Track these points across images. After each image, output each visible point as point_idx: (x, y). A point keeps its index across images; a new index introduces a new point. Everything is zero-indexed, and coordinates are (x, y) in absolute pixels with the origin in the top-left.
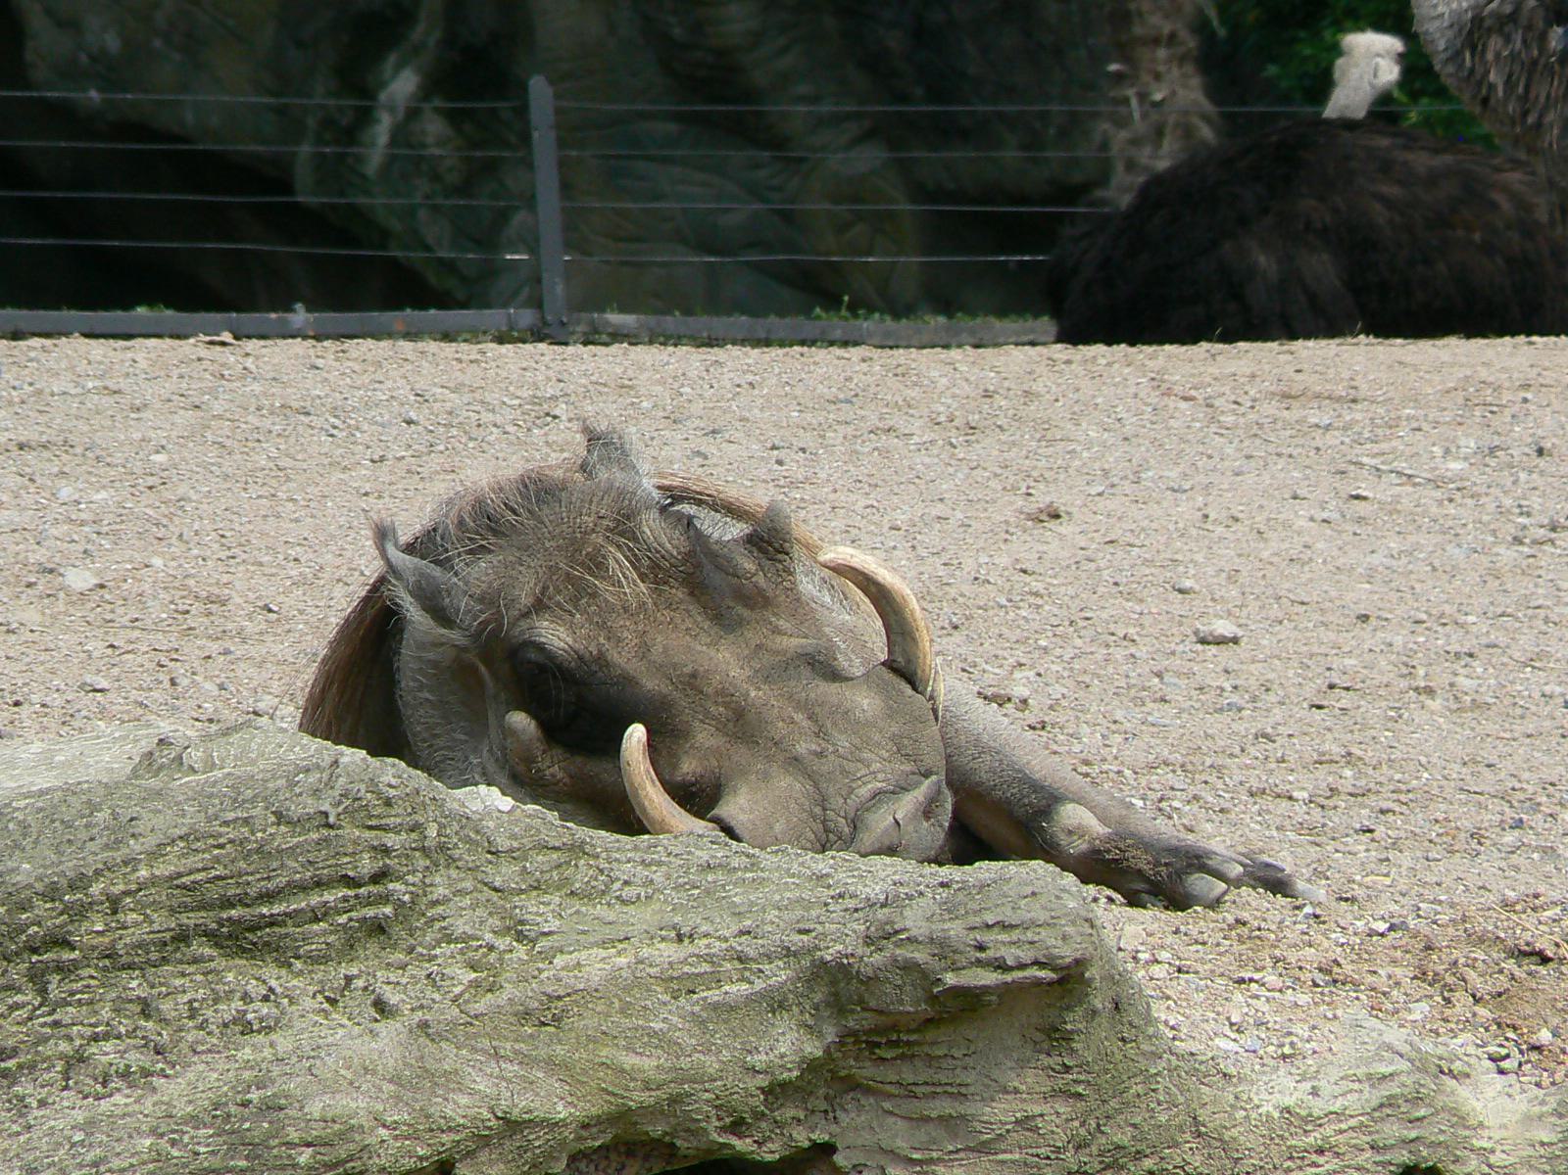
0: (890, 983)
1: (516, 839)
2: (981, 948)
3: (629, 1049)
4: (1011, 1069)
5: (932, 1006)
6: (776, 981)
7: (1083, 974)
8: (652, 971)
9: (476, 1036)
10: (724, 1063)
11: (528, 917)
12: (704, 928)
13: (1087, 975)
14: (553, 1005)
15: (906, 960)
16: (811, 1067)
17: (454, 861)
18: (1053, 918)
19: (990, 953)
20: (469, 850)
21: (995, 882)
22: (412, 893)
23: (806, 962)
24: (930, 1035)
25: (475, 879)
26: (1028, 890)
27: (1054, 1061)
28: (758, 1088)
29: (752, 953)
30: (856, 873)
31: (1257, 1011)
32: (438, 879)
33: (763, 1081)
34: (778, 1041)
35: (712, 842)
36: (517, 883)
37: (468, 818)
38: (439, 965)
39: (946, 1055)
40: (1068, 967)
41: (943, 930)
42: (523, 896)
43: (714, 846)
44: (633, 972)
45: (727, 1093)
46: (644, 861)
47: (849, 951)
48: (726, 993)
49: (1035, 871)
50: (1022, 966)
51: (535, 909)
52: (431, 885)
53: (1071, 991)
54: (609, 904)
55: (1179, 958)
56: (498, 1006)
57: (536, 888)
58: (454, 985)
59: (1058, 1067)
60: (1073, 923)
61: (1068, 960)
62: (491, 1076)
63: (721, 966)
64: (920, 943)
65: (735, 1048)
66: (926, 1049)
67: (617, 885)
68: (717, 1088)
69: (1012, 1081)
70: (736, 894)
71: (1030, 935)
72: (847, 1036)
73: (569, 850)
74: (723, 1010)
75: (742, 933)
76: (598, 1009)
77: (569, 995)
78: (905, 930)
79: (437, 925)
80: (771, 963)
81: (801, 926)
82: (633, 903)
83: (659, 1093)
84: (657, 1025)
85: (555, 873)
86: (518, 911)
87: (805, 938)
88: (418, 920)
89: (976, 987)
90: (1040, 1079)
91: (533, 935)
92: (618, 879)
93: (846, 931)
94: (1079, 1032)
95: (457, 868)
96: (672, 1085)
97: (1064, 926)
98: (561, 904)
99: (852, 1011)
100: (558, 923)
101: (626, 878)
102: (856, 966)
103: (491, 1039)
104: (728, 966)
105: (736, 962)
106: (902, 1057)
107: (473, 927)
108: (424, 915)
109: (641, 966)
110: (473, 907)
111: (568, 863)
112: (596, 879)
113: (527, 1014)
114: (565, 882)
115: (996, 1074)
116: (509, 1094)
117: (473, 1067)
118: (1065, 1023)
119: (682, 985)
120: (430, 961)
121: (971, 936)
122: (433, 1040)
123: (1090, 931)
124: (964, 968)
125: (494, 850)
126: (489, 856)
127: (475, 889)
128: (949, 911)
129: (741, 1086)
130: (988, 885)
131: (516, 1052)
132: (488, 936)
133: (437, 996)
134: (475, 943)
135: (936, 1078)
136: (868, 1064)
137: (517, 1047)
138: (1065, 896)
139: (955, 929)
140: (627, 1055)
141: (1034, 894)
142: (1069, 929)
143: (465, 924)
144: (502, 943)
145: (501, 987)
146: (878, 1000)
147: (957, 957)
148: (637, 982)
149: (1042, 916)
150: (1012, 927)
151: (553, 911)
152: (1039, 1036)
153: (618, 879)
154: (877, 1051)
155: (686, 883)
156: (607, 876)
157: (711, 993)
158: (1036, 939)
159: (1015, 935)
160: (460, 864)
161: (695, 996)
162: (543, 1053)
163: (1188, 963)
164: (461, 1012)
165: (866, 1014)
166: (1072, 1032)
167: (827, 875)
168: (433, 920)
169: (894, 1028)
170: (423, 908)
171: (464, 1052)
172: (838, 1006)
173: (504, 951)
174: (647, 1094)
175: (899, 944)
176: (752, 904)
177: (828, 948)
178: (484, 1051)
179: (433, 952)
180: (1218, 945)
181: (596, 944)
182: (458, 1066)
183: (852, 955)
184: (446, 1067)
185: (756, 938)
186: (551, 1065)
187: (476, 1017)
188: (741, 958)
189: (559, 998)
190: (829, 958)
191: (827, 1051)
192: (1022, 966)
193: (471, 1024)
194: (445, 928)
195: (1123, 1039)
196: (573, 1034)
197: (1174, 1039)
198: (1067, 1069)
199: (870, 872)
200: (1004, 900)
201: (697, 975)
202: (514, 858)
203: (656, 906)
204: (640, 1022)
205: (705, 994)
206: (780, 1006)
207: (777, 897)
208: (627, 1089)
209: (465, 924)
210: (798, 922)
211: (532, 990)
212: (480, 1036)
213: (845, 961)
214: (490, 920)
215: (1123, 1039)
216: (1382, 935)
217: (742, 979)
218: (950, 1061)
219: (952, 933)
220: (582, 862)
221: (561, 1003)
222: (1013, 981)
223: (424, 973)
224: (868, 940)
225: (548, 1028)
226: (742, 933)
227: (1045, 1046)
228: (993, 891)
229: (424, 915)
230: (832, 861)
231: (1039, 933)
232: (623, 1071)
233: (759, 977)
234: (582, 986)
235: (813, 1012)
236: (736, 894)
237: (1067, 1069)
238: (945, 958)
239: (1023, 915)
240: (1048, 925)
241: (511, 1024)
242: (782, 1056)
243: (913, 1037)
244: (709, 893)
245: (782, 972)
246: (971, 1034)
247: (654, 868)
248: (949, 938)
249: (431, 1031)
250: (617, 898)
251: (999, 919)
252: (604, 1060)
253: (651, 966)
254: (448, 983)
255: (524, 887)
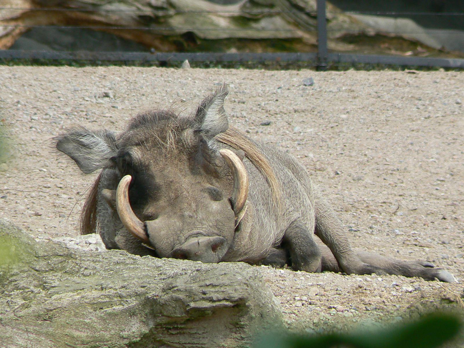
0: (171, 306)
1: (47, 252)
2: (204, 293)
3: (77, 329)
4: (221, 338)
5: (188, 314)
6: (132, 305)
7: (245, 304)
8: (87, 301)
9: (20, 324)
10: (112, 335)
11: (48, 281)
12: (110, 286)
13: (247, 304)
14: (49, 313)
15: (176, 298)
16: (145, 337)
17: (21, 260)
18: (231, 283)
19: (208, 296)
20: (28, 256)
21: (212, 269)
22: (3, 271)
23: (143, 298)
24: (189, 325)
25: (29, 266)
26: (223, 272)
27: (238, 336)
28: (125, 344)
29: (124, 294)
30: (171, 266)
31: (326, 318)
32: (14, 266)
33: (126, 342)
34: (132, 327)
35: (120, 254)
36: (45, 268)
37: (29, 244)
38: (12, 298)
39: (196, 333)
40: (237, 301)
41: (190, 287)
42: (47, 273)
43: (121, 255)
44: (79, 302)
45: (113, 346)
46: (93, 260)
47: (157, 294)
48: (114, 309)
49: (238, 266)
50: (219, 300)
51: (51, 278)
52: (12, 269)
53: (242, 310)
54: (79, 276)
55: (311, 299)
56: (28, 313)
57: (52, 270)
58: (15, 305)
59: (239, 338)
60: (240, 285)
61: (236, 298)
62: (24, 339)
63: (113, 299)
64: (182, 291)
65: (116, 330)
66: (188, 331)
67: (82, 269)
68: (109, 344)
69: (222, 343)
70: (126, 273)
71: (222, 289)
72: (157, 325)
73: (66, 256)
74: (113, 316)
75: (122, 287)
76: (66, 315)
77: (55, 309)
78: (177, 286)
79: (13, 283)
80: (131, 298)
81: (143, 285)
82: (88, 276)
83: (87, 346)
84: (87, 321)
85: (60, 265)
86: (44, 278)
87: (143, 289)
88: (6, 281)
89: (202, 308)
90: (232, 342)
91: (48, 287)
92: (83, 267)
93: (157, 287)
94: (246, 325)
95: (23, 262)
96: (92, 343)
97: (236, 286)
98: (61, 276)
99: (159, 317)
100: (58, 283)
101: (86, 267)
102: (159, 300)
103: (25, 325)
104: (116, 299)
105: (118, 298)
106: (180, 333)
107: (27, 284)
108: (8, 279)
109: (83, 299)
110: (27, 277)
111: (65, 261)
112: (75, 267)
113: (39, 316)
114: (63, 268)
115: (215, 340)
116: (31, 345)
117: (18, 335)
118: (241, 321)
119: (97, 306)
120: (9, 296)
121: (201, 289)
122: (3, 325)
123: (247, 288)
124: (198, 301)
125: (37, 256)
126: (35, 258)
127: (29, 270)
128: (194, 280)
129: (118, 343)
130: (209, 271)
131: (35, 330)
132: (32, 288)
133: (8, 309)
134: (27, 290)
135: (193, 341)
136: (167, 336)
137: (35, 328)
138: (237, 275)
139: (195, 287)
140: (75, 332)
141: (225, 274)
142: (238, 287)
143: (24, 283)
144: (36, 290)
145: (31, 306)
146: (167, 312)
147: (195, 297)
148: (81, 305)
149: (227, 282)
150: (216, 286)
151: (58, 279)
152: (231, 326)
153: (83, 267)
154: (170, 331)
155: (108, 269)
156: (79, 266)
157: (108, 309)
158: (224, 290)
159: (217, 289)
160: (23, 261)
161: (103, 310)
162: (45, 330)
163: (314, 301)
164: (15, 315)
165: (164, 317)
166: (243, 325)
167: (160, 267)
168: (11, 281)
169: (175, 323)
170: (8, 277)
171: (15, 330)
172: (154, 314)
173: (37, 293)
174: (83, 346)
175: (174, 292)
176: (130, 277)
177: (150, 293)
178: (23, 330)
179: (10, 293)
180: (345, 295)
181: (71, 291)
182: (12, 335)
183: (158, 295)
184: (7, 335)
185: (126, 289)
186: (48, 335)
187: (20, 317)
188: (121, 296)
189: (51, 310)
190: (150, 297)
191: (150, 330)
192: (219, 300)
193: (18, 320)
194: (16, 284)
195: (264, 328)
196: (56, 324)
197: (289, 328)
198: (243, 339)
199: (177, 265)
200: (214, 276)
201: (103, 302)
202: (45, 259)
203: (96, 277)
204: (81, 320)
205: (106, 309)
206: (133, 314)
207: (139, 274)
208: (75, 344)
209: (24, 283)
210: (142, 283)
211: (41, 307)
212: (21, 324)
213: (155, 298)
214: (34, 282)
215: (264, 328)
216: (411, 292)
217: (121, 304)
218: (198, 335)
219: (193, 288)
220: (70, 261)
221: (52, 312)
222: (216, 306)
223: (6, 301)
224: (164, 290)
225: (47, 322)
226: (122, 287)
227: (234, 330)
228: (210, 273)
229: (8, 279)
230: (164, 261)
231: (226, 288)
232: (74, 337)
233: (126, 304)
234: (60, 306)
235: (145, 316)
236: (126, 273)
237: (243, 339)
238: (191, 297)
239: (220, 282)
240: (230, 285)
241: (33, 320)
242: (133, 333)
243: (183, 326)
244: (116, 272)
245: (134, 302)
246: (205, 326)
247: (97, 263)
248: (192, 290)
249: (2, 322)
250: (82, 274)
251: (211, 283)
252: (67, 333)
253: (86, 299)
254: (14, 304)
255: (47, 270)
